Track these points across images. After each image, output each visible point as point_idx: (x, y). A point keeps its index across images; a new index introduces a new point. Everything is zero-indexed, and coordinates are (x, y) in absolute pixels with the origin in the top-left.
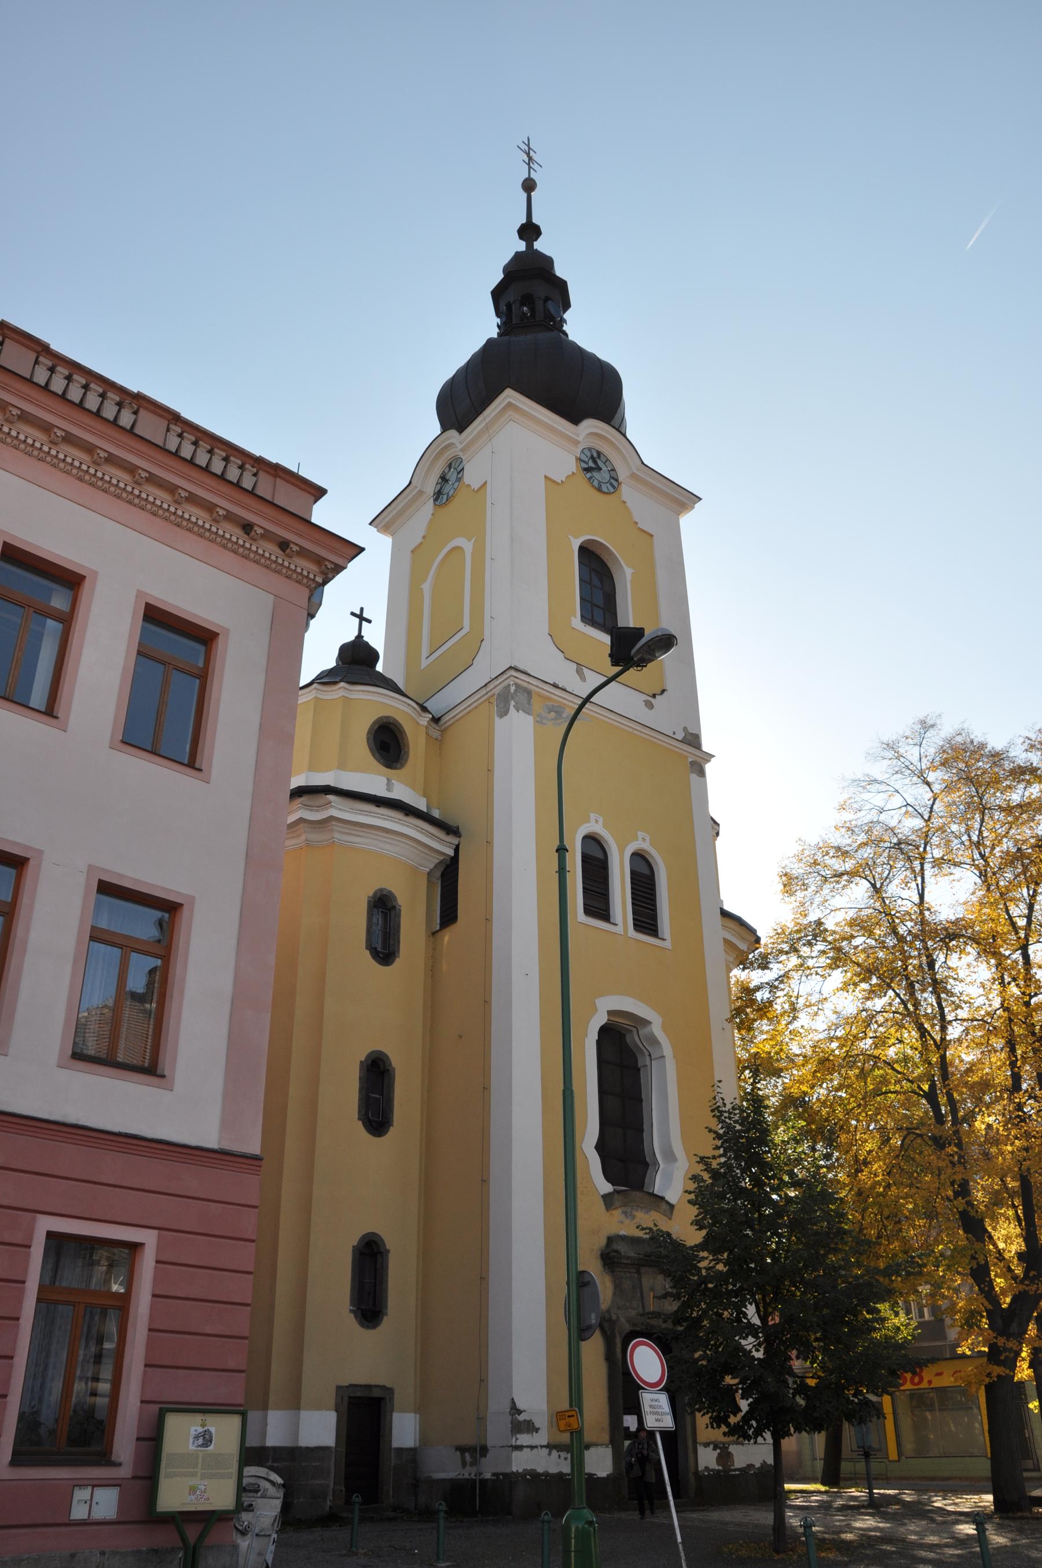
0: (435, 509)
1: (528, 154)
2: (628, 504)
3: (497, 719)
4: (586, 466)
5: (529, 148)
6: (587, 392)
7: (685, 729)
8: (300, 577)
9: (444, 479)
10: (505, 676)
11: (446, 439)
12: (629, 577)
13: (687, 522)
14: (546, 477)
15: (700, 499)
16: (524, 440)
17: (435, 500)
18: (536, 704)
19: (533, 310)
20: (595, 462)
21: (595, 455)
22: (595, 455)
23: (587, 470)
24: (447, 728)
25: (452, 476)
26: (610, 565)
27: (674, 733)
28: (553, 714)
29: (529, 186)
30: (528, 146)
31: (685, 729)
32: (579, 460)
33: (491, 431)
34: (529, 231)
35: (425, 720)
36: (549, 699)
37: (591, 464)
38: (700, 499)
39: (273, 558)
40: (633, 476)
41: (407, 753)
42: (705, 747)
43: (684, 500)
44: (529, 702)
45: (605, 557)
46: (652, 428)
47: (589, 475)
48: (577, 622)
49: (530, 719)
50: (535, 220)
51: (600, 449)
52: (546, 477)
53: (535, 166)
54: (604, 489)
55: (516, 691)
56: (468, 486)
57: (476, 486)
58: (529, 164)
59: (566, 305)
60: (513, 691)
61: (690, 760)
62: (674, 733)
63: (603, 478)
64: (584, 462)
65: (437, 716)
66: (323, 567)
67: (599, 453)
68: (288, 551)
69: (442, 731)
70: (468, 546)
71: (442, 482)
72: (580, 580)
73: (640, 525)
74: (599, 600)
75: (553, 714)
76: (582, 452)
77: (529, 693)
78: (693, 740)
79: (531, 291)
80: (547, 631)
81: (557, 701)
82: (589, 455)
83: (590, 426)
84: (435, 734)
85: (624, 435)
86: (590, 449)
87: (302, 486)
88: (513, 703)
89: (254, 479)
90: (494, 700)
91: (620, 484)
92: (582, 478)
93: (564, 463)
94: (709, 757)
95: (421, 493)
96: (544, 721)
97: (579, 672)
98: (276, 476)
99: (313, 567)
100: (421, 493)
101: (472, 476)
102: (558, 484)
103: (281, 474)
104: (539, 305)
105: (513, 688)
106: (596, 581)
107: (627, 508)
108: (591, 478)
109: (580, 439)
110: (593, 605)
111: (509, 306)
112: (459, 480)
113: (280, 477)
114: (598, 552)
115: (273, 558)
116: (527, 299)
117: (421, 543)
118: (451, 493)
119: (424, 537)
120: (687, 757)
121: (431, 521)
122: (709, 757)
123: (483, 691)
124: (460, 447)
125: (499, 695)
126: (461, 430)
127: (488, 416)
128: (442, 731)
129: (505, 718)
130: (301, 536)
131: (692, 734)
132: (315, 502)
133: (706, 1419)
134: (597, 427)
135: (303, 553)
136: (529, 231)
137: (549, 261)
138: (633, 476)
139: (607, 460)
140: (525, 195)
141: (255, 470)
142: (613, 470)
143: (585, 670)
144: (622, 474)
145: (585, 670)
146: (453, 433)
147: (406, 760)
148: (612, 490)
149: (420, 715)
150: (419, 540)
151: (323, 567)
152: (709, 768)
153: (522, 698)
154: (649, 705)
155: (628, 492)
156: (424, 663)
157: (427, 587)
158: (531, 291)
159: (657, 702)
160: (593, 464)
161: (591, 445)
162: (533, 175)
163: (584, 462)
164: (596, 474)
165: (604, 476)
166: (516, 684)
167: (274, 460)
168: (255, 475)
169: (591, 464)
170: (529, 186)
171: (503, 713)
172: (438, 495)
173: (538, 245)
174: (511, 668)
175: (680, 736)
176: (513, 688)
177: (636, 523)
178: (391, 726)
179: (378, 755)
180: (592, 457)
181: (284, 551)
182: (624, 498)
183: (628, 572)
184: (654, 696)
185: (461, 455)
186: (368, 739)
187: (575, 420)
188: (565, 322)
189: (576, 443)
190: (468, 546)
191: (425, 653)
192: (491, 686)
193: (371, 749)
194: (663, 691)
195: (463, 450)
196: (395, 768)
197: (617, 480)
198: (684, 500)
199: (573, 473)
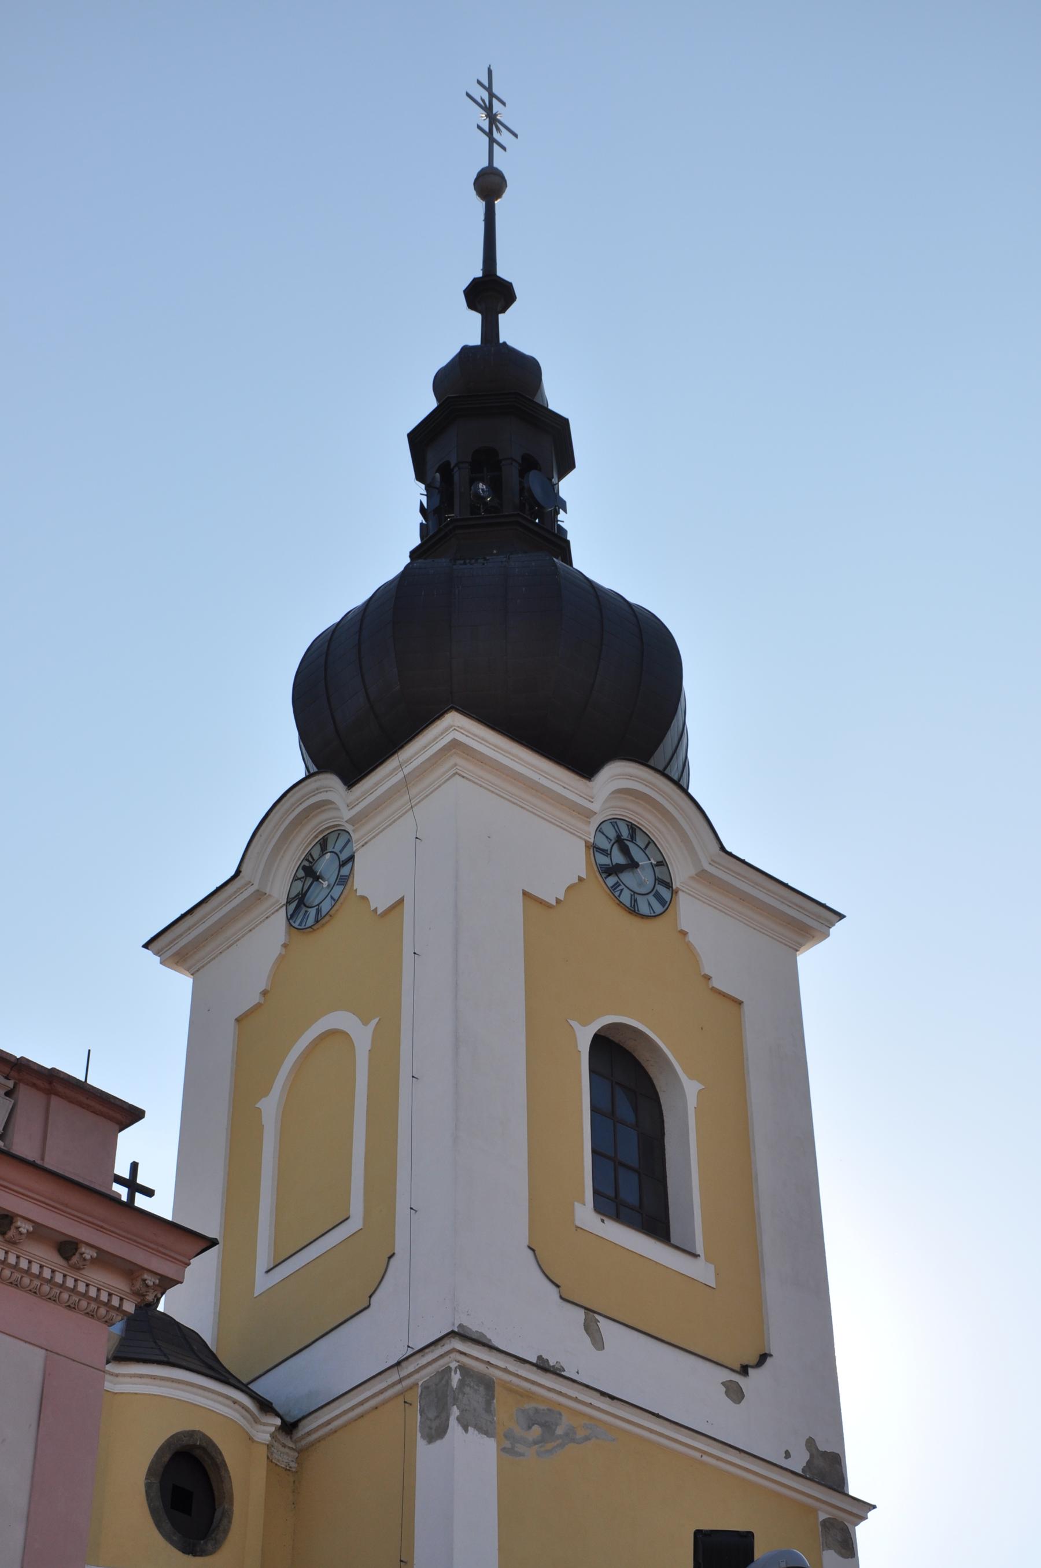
0: (288, 933)
1: (488, 110)
2: (691, 938)
3: (421, 1443)
4: (604, 860)
5: (492, 95)
6: (605, 691)
7: (810, 1443)
8: (93, 1305)
9: (309, 872)
10: (439, 1351)
11: (317, 791)
12: (692, 1101)
13: (812, 963)
14: (525, 894)
15: (841, 916)
16: (477, 814)
17: (290, 918)
18: (504, 1410)
19: (496, 487)
20: (625, 851)
21: (625, 833)
22: (625, 833)
23: (609, 871)
24: (312, 1444)
25: (326, 865)
26: (653, 1071)
27: (787, 1455)
28: (537, 1430)
29: (490, 185)
30: (489, 89)
31: (810, 1443)
32: (594, 848)
33: (413, 791)
34: (489, 294)
35: (266, 1429)
36: (529, 1396)
37: (618, 858)
38: (841, 916)
39: (47, 1274)
40: (703, 876)
41: (228, 1515)
42: (856, 1487)
43: (806, 919)
44: (489, 1403)
45: (643, 1056)
46: (743, 771)
47: (612, 880)
48: (586, 1215)
49: (490, 1445)
50: (503, 271)
51: (635, 820)
52: (525, 894)
53: (503, 137)
54: (644, 908)
55: (462, 1383)
56: (364, 898)
57: (380, 902)
58: (490, 134)
59: (567, 464)
60: (454, 1383)
61: (822, 1516)
62: (787, 1455)
63: (641, 884)
64: (604, 852)
65: (290, 1419)
66: (138, 1284)
67: (633, 828)
68: (75, 1259)
69: (300, 1451)
70: (362, 1036)
71: (303, 874)
72: (594, 1109)
73: (715, 983)
74: (630, 1153)
75: (537, 1430)
76: (599, 829)
77: (488, 1385)
78: (828, 1469)
79: (491, 440)
80: (526, 1242)
81: (545, 1400)
82: (612, 834)
83: (617, 775)
84: (285, 1457)
85: (685, 791)
86: (614, 822)
87: (99, 1107)
88: (455, 1412)
89: (9, 1103)
90: (414, 1397)
91: (674, 892)
92: (597, 890)
93: (562, 860)
94: (862, 1509)
95: (260, 896)
96: (520, 1448)
97: (591, 1329)
98: (49, 1092)
99: (119, 1284)
100: (260, 896)
101: (375, 876)
102: (549, 906)
103: (60, 1088)
104: (511, 473)
105: (456, 1378)
106: (625, 1110)
107: (689, 946)
108: (616, 886)
109: (596, 807)
110: (619, 1164)
111: (446, 470)
112: (344, 880)
113: (57, 1094)
114: (629, 1045)
115: (47, 1274)
116: (485, 462)
117: (258, 1006)
118: (325, 907)
119: (264, 993)
120: (814, 1511)
121: (281, 958)
122: (862, 1509)
123: (394, 1376)
124: (347, 814)
125: (426, 1387)
126: (350, 780)
127: (409, 761)
128: (300, 1451)
129: (439, 1442)
130: (100, 1228)
131: (825, 1454)
132: (120, 1131)
133: (130, 1147)
134: (631, 777)
135: (105, 1260)
136: (489, 294)
137: (527, 371)
138: (703, 876)
139: (650, 842)
140: (480, 205)
141: (10, 1084)
142: (662, 863)
143: (603, 1324)
144: (681, 873)
145: (603, 1324)
146: (331, 784)
147: (226, 1532)
148: (658, 908)
149: (256, 1421)
150: (255, 998)
151: (138, 1284)
152: (863, 1533)
153: (475, 1398)
154: (735, 1393)
155: (692, 911)
156: (262, 1283)
157: (270, 1107)
158: (491, 440)
159: (754, 1383)
160: (624, 859)
161: (618, 813)
162: (500, 162)
163: (604, 852)
164: (627, 878)
165: (642, 879)
166: (464, 1369)
167: (47, 1062)
168: (9, 1094)
169: (618, 858)
170: (490, 185)
171: (436, 1432)
172: (298, 903)
173: (515, 330)
174: (452, 1334)
175: (799, 1462)
176: (456, 1378)
177: (708, 978)
178: (197, 1453)
179: (167, 1526)
180: (619, 841)
181: (67, 1258)
182: (684, 925)
183: (691, 1088)
184: (744, 1370)
185: (349, 828)
186: (148, 1486)
187: (586, 768)
188: (562, 505)
189: (587, 814)
190: (362, 1036)
191: (263, 1260)
192: (409, 1367)
193: (153, 1512)
194: (763, 1358)
195: (352, 821)
196: (202, 1553)
197: (668, 885)
198: (806, 919)
199: (580, 879)
